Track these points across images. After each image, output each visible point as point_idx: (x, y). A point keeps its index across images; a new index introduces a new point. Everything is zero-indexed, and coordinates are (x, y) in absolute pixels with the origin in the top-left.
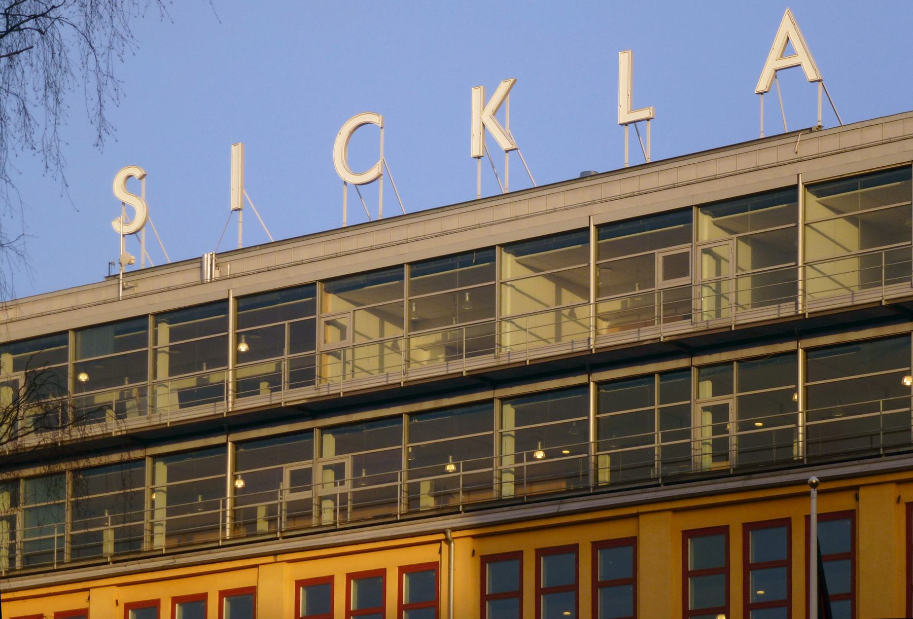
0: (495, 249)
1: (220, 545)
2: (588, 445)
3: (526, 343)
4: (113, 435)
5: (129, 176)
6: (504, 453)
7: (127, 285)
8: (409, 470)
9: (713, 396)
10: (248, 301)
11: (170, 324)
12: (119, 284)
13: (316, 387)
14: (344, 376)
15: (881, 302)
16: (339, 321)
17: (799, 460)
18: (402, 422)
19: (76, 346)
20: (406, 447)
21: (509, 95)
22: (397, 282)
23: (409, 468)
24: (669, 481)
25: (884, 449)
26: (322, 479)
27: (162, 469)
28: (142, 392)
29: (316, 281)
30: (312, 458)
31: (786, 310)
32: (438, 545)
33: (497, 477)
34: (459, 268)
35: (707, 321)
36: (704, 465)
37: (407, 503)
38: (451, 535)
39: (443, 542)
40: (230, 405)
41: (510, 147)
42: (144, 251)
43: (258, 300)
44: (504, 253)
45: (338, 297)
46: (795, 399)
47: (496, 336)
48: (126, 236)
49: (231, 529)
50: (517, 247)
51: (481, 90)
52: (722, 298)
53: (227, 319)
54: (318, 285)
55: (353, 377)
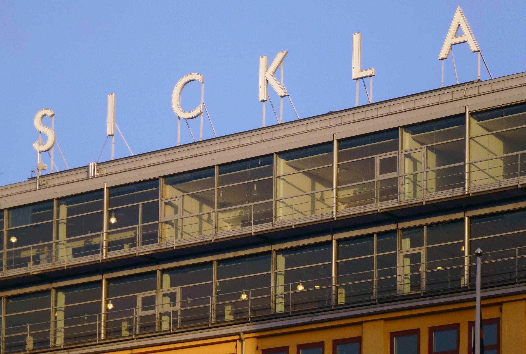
0: (273, 155)
1: (97, 343)
2: (331, 280)
3: (292, 214)
4: (31, 274)
5: (44, 115)
6: (277, 284)
7: (42, 183)
8: (217, 295)
9: (171, 287)
10: (115, 190)
11: (67, 205)
12: (37, 182)
13: (53, 263)
14: (176, 238)
15: (517, 186)
16: (173, 202)
17: (465, 287)
18: (213, 264)
19: (9, 220)
20: (215, 282)
21: (283, 61)
22: (211, 177)
23: (217, 294)
24: (382, 301)
25: (519, 279)
26: (162, 302)
27: (61, 296)
28: (50, 246)
29: (159, 177)
30: (155, 289)
31: (458, 192)
32: (235, 343)
33: (273, 300)
34: (250, 168)
35: (408, 200)
36: (404, 292)
37: (216, 317)
38: (243, 336)
39: (238, 341)
40: (104, 255)
41: (283, 94)
42: (52, 162)
43: (123, 189)
44: (279, 158)
45: (173, 187)
46: (463, 250)
47: (273, 210)
48: (42, 153)
49: (104, 334)
50: (286, 154)
51: (265, 58)
52: (417, 186)
53: (103, 202)
54: (161, 179)
55: (182, 238)
